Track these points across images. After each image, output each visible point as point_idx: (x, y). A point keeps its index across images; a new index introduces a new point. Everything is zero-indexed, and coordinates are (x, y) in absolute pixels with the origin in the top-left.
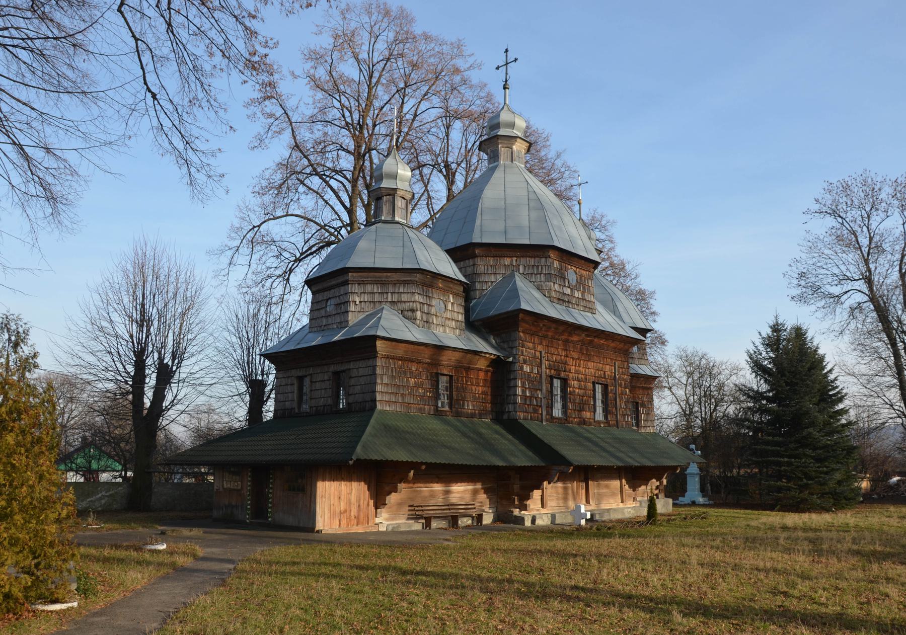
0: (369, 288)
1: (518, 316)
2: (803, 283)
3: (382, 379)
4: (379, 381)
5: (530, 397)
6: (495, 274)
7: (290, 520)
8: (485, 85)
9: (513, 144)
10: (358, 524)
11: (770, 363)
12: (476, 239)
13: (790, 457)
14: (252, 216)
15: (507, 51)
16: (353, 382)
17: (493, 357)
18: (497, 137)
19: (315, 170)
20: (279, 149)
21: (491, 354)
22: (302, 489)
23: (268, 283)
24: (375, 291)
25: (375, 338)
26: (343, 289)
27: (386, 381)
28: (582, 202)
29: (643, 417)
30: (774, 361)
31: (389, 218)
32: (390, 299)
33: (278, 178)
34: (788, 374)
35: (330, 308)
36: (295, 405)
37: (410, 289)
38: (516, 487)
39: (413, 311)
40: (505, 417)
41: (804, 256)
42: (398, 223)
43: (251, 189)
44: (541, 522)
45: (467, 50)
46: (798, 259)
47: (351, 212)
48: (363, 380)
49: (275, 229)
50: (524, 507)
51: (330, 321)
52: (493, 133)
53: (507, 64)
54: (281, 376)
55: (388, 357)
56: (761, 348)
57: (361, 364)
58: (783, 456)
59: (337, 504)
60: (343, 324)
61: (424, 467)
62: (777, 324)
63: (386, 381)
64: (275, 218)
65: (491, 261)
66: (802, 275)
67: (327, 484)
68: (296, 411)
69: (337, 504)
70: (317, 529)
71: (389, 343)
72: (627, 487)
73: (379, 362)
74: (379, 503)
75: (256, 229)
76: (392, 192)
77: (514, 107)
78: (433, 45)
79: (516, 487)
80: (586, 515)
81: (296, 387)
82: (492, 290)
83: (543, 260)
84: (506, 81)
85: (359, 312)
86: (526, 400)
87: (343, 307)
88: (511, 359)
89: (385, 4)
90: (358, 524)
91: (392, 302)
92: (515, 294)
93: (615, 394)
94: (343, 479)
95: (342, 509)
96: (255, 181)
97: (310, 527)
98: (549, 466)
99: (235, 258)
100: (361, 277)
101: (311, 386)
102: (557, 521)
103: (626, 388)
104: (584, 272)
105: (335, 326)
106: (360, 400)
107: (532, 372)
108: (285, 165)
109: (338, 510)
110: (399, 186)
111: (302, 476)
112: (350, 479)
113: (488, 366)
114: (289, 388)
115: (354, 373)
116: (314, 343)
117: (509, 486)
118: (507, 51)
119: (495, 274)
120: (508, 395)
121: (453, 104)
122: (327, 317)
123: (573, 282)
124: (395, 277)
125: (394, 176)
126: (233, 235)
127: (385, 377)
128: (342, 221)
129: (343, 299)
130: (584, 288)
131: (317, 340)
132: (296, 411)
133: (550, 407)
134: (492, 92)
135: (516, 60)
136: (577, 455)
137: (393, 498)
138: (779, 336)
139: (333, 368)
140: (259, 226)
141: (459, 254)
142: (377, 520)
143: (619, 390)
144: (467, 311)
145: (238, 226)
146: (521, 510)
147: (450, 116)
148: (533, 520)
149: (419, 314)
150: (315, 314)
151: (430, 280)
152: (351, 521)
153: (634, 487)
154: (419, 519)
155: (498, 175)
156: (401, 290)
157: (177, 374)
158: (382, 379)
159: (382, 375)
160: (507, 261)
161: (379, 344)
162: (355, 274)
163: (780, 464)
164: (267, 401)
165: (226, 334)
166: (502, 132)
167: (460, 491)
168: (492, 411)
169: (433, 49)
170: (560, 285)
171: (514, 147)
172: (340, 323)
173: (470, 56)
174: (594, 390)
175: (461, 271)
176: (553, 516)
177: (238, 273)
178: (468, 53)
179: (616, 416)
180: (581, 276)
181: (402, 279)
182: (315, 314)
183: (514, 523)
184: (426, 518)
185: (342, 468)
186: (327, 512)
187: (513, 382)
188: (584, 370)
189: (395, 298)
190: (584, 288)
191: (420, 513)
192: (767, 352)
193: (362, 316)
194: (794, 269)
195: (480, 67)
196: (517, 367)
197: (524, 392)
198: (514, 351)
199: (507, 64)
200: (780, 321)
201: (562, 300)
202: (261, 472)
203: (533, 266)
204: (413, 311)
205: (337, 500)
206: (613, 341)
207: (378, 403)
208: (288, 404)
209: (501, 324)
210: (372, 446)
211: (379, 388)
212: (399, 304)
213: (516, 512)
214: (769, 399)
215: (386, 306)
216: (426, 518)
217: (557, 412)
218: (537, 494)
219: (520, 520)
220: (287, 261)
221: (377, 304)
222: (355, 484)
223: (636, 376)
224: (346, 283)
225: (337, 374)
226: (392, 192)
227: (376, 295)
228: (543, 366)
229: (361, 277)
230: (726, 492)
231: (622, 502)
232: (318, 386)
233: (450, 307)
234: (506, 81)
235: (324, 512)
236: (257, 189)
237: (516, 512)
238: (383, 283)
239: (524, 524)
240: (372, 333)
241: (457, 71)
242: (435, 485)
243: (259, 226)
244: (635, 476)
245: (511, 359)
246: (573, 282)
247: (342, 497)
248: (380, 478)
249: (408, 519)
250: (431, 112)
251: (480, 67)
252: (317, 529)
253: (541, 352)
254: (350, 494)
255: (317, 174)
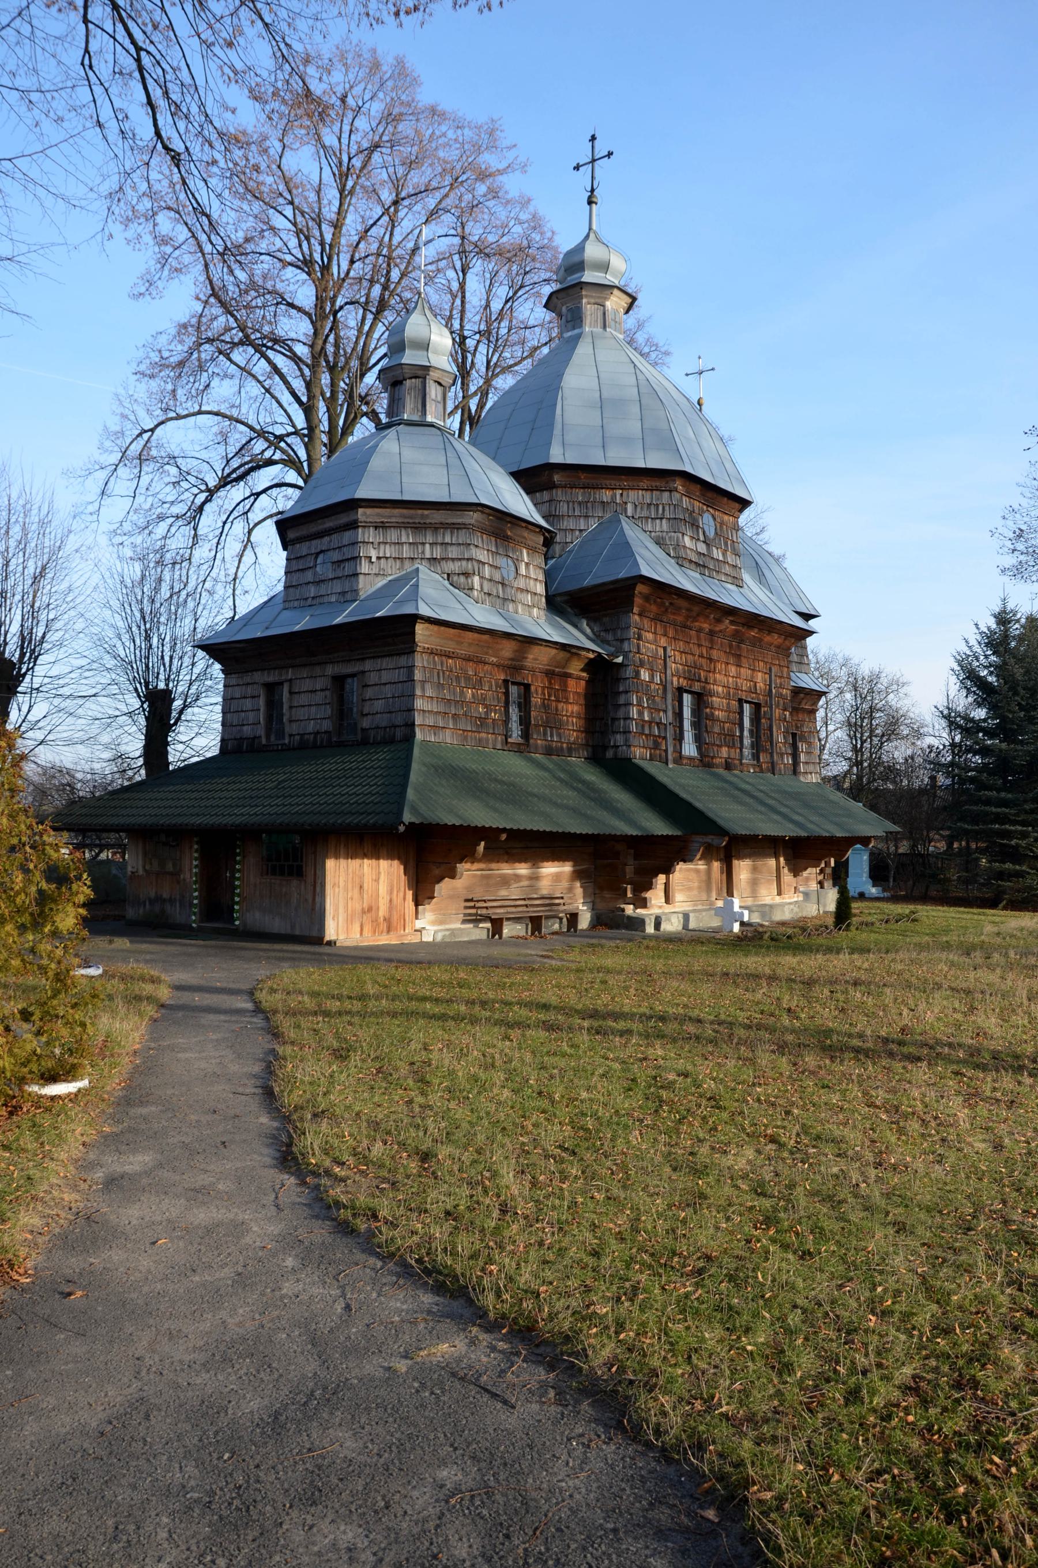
0: (393, 535)
1: (633, 587)
2: (1021, 546)
3: (423, 689)
4: (418, 692)
5: (650, 722)
6: (587, 517)
7: (277, 925)
8: (529, 200)
9: (607, 299)
10: (388, 931)
11: (991, 673)
12: (556, 456)
13: (1023, 824)
14: (142, 413)
15: (593, 138)
16: (369, 693)
17: (591, 656)
18: (581, 285)
19: (247, 336)
20: (182, 298)
21: (588, 650)
22: (298, 872)
23: (161, 529)
24: (404, 539)
25: (414, 619)
26: (347, 536)
27: (429, 692)
28: (703, 401)
29: (803, 757)
30: (1000, 670)
31: (416, 418)
32: (428, 555)
33: (178, 351)
34: (1022, 692)
35: (323, 569)
36: (261, 731)
37: (462, 537)
38: (629, 871)
39: (466, 575)
40: (610, 754)
41: (1025, 502)
42: (431, 425)
43: (134, 367)
44: (672, 925)
45: (506, 138)
46: (1016, 507)
47: (308, 410)
48: (388, 691)
49: (175, 437)
50: (643, 903)
51: (323, 589)
52: (572, 279)
53: (593, 161)
54: (233, 682)
55: (432, 653)
56: (977, 649)
57: (386, 663)
58: (1014, 823)
59: (360, 897)
60: (349, 595)
61: (504, 837)
62: (1005, 612)
63: (429, 692)
64: (179, 417)
65: (580, 495)
66: (1020, 534)
67: (343, 862)
68: (264, 741)
69: (360, 897)
70: (327, 938)
71: (435, 628)
72: (786, 870)
73: (420, 660)
74: (422, 894)
75: (146, 436)
76: (420, 373)
77: (604, 235)
78: (444, 128)
79: (629, 871)
80: (742, 914)
81: (262, 702)
82: (582, 545)
83: (666, 494)
84: (592, 190)
85: (382, 572)
86: (643, 726)
87: (347, 565)
88: (620, 660)
89: (374, 51)
90: (388, 931)
91: (433, 560)
92: (625, 549)
93: (770, 719)
94: (365, 856)
95: (365, 905)
96: (141, 354)
97: (318, 940)
98: (697, 835)
99: (110, 485)
100: (378, 515)
101: (290, 700)
102: (692, 925)
103: (785, 710)
104: (726, 518)
105: (333, 599)
106: (384, 724)
107: (652, 681)
108: (196, 330)
109: (358, 907)
110: (434, 363)
111: (295, 854)
112: (375, 854)
113: (582, 670)
114: (248, 704)
115: (373, 678)
116: (297, 628)
117: (618, 867)
118: (593, 138)
119: (587, 517)
120: (614, 719)
121: (475, 231)
122: (318, 583)
123: (711, 534)
124: (437, 517)
125: (424, 346)
126: (108, 444)
127: (428, 686)
128: (294, 426)
129: (348, 553)
130: (726, 544)
131: (303, 622)
132: (264, 741)
133: (680, 738)
134: (541, 213)
135: (610, 154)
136: (737, 817)
137: (444, 888)
138: (1007, 630)
139: (330, 670)
140: (152, 430)
141: (533, 479)
142: (419, 924)
143: (777, 713)
144: (549, 577)
145: (118, 428)
146: (636, 908)
147: (467, 251)
148: (658, 925)
149: (476, 579)
150: (296, 578)
151: (501, 525)
152: (378, 925)
153: (796, 872)
154: (480, 921)
155: (583, 349)
156: (448, 539)
157: (28, 678)
158: (423, 689)
159: (423, 682)
160: (606, 495)
161: (420, 629)
162: (369, 511)
163: (1008, 835)
164: (175, 724)
165: (108, 613)
166: (588, 276)
167: (554, 874)
168: (587, 745)
169: (444, 135)
170: (692, 538)
171: (608, 304)
172: (343, 593)
173: (509, 148)
174: (741, 713)
175: (539, 511)
176: (686, 917)
177: (116, 509)
178: (507, 143)
179: (772, 754)
180: (722, 524)
181: (450, 521)
182: (296, 578)
183: (627, 928)
184: (493, 921)
185: (369, 838)
186: (341, 910)
187: (622, 710)
188: (730, 679)
189: (438, 553)
190: (726, 544)
191: (484, 912)
192: (986, 657)
193: (381, 582)
194: (1010, 523)
195: (524, 168)
196: (629, 672)
197: (641, 713)
198: (626, 646)
199: (593, 161)
200: (1010, 606)
201: (701, 565)
202: (219, 845)
203: (649, 505)
204: (466, 575)
205: (357, 890)
206: (770, 632)
207: (417, 730)
208: (247, 731)
209: (599, 601)
210: (428, 800)
211: (419, 704)
212: (443, 563)
213: (629, 910)
214: (987, 732)
215: (424, 569)
216: (493, 921)
217: (689, 749)
218: (661, 878)
219: (638, 924)
220: (195, 491)
221: (407, 563)
222: (384, 864)
223: (799, 692)
224: (354, 525)
225: (339, 681)
226: (422, 372)
227: (405, 547)
228: (669, 672)
229: (378, 515)
230: (907, 877)
231: (779, 893)
232: (304, 699)
233: (523, 570)
234: (592, 190)
235: (337, 910)
236: (142, 368)
237: (629, 910)
238: (418, 528)
239: (644, 931)
240: (408, 609)
241: (483, 176)
242: (504, 865)
243: (152, 430)
244: (799, 852)
245: (620, 660)
246: (711, 534)
247: (365, 886)
248: (429, 854)
249: (464, 922)
250: (437, 240)
251: (524, 168)
252: (327, 938)
253: (665, 649)
254: (377, 880)
255: (251, 344)
